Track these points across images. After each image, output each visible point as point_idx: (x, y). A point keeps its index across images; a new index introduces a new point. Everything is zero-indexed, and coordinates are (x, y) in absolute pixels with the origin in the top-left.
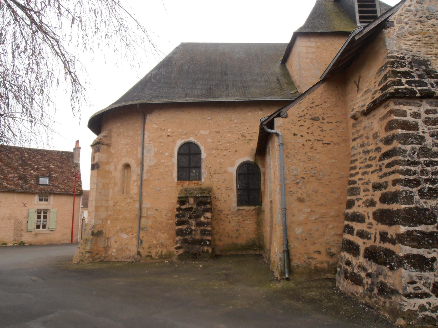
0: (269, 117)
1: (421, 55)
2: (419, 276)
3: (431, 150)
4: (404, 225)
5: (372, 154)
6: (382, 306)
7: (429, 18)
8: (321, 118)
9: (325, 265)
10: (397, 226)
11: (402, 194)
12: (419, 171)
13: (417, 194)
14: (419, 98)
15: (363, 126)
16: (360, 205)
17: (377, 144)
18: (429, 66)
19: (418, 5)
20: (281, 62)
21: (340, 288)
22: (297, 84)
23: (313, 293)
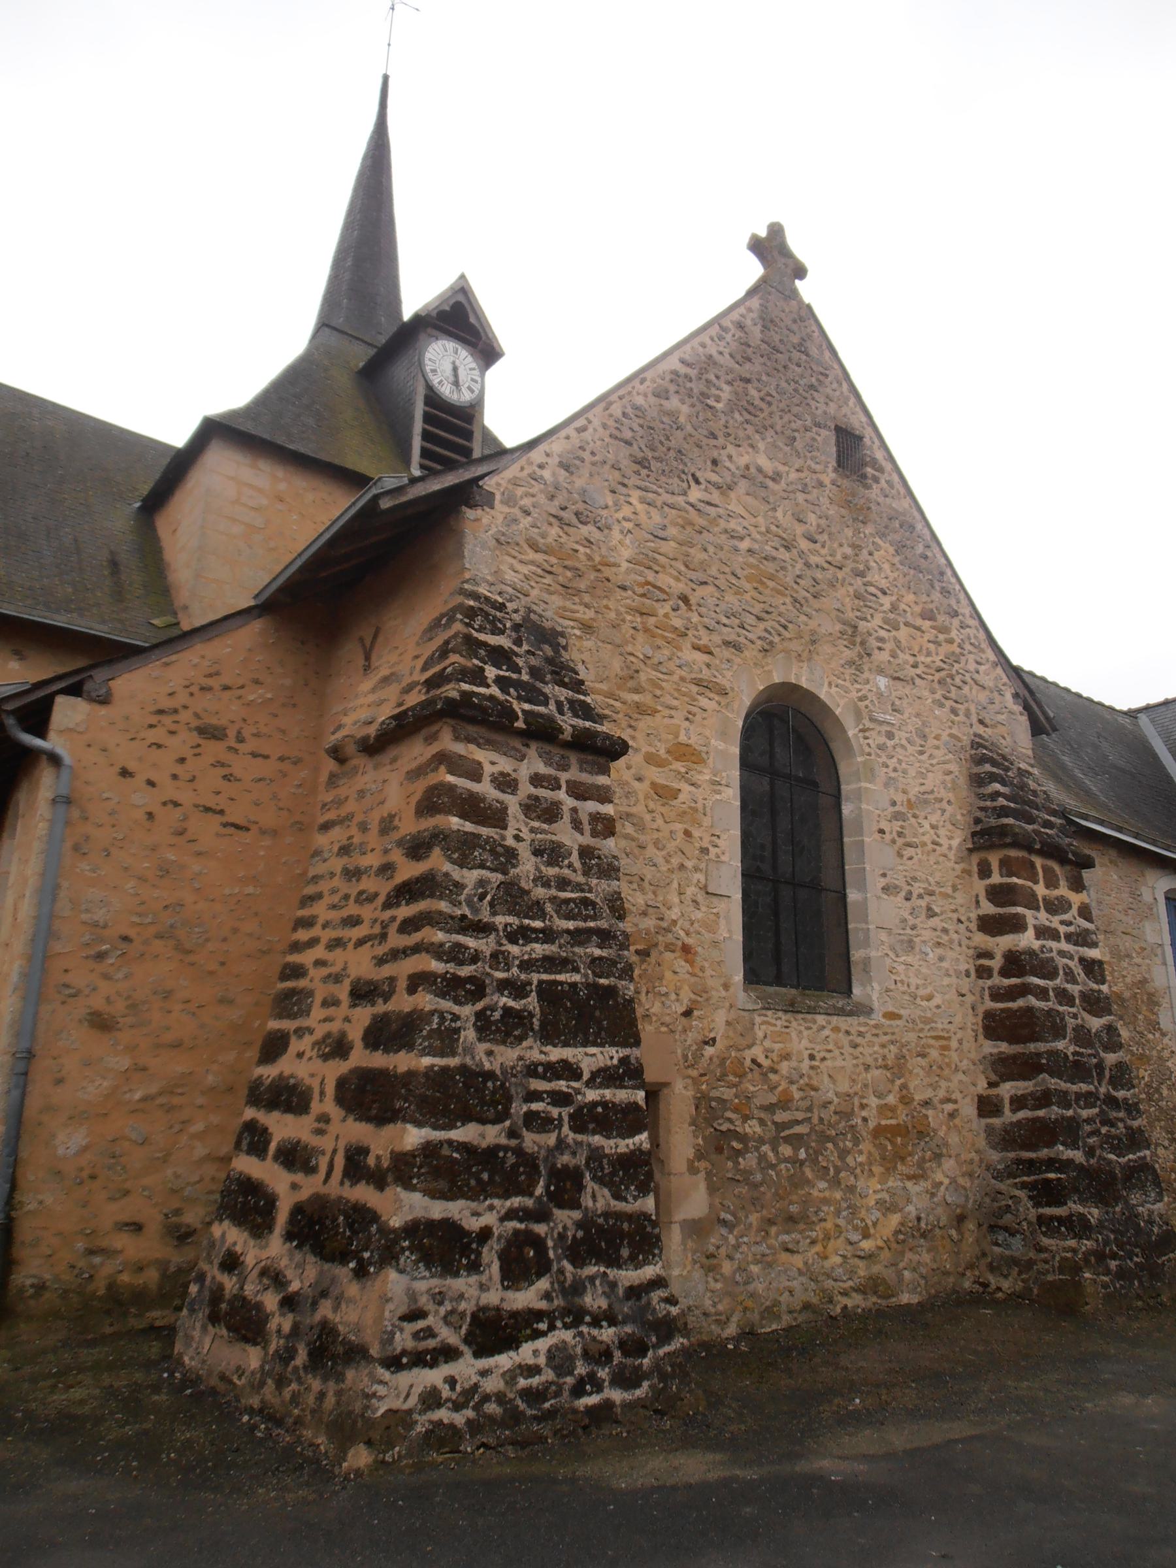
0: (34, 685)
1: (548, 614)
2: (437, 1290)
3: (528, 892)
4: (419, 1124)
5: (369, 884)
6: (313, 1411)
7: (583, 519)
8: (232, 733)
9: (152, 1276)
10: (399, 1124)
11: (429, 1023)
12: (488, 954)
13: (470, 1024)
14: (520, 733)
15: (359, 787)
16: (303, 1053)
17: (386, 851)
18: (563, 652)
19: (563, 472)
20: (138, 505)
21: (186, 1359)
22: (182, 596)
23: (77, 1393)
